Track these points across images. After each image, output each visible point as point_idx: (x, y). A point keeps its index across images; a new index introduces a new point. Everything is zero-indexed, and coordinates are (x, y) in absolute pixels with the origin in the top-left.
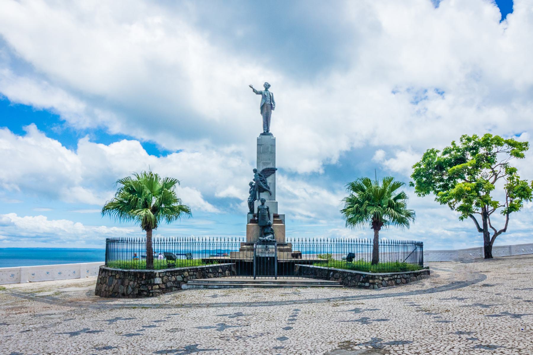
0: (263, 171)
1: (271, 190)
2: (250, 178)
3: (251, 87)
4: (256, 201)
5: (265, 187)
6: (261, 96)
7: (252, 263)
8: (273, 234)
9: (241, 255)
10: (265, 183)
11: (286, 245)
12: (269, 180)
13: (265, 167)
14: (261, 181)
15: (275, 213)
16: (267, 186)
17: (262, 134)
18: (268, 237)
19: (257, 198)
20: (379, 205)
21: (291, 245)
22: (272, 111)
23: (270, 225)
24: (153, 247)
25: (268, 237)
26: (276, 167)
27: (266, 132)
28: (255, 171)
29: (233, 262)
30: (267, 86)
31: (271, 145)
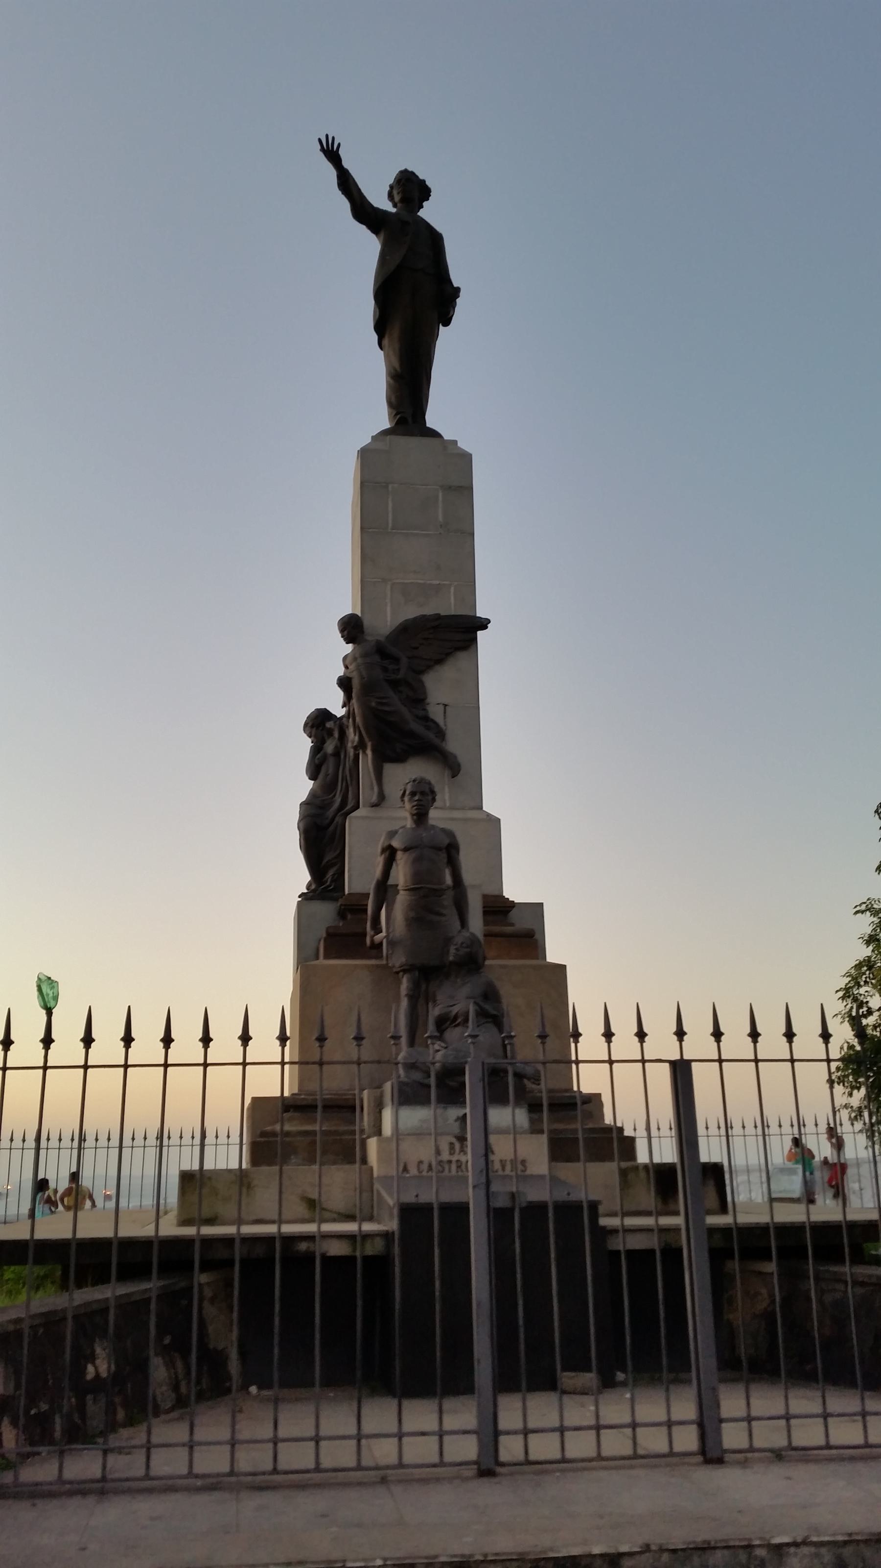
0: (407, 630)
1: (453, 745)
2: (319, 677)
3: (332, 154)
5: (417, 727)
7: (393, 1233)
9: (265, 1198)
10: (418, 700)
12: (438, 686)
13: (411, 612)
14: (394, 684)
15: (490, 890)
16: (426, 720)
17: (385, 433)
18: (470, 1046)
20: (499, 1085)
22: (442, 328)
26: (481, 612)
27: (49, 1012)
28: (351, 628)
29: (128, 1273)
31: (448, 489)
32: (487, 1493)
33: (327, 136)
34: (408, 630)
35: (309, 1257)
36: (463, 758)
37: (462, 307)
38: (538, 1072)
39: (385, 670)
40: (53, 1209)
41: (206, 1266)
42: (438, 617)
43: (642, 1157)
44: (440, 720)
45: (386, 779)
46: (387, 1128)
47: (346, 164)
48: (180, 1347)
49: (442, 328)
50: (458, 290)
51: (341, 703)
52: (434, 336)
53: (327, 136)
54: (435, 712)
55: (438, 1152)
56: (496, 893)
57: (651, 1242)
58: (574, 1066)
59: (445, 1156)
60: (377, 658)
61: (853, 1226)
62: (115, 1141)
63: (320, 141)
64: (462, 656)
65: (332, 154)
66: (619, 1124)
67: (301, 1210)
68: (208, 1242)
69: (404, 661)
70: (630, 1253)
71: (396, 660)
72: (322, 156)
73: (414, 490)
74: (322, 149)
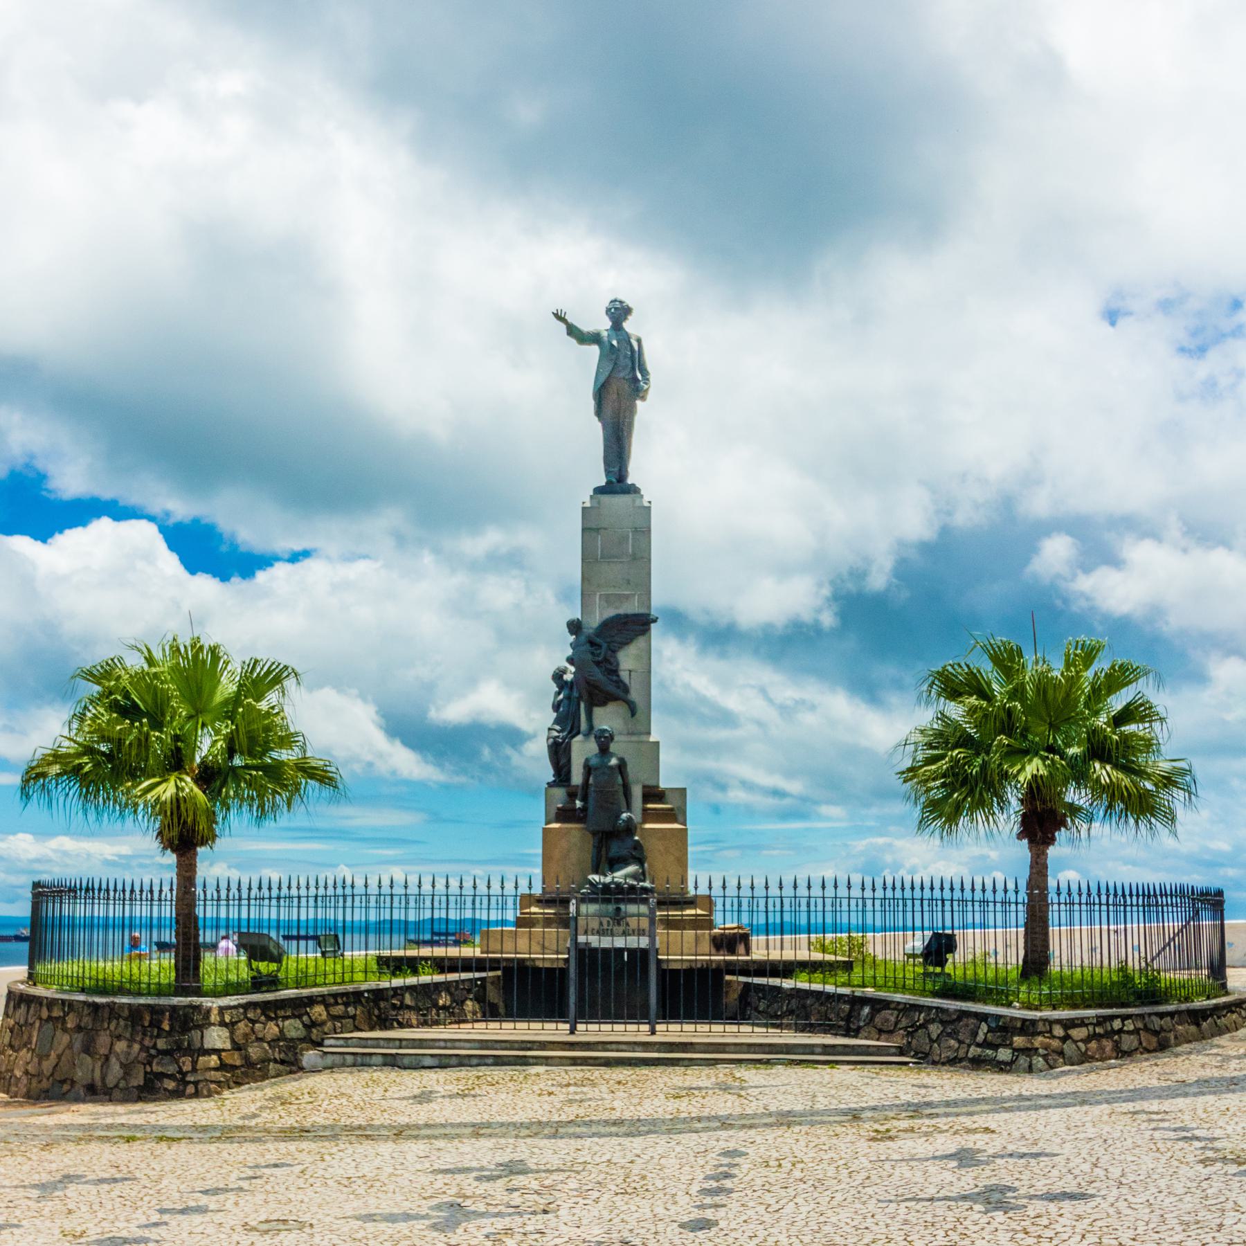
0: (607, 625)
1: (634, 695)
3: (559, 317)
4: (579, 738)
6: (595, 350)
8: (640, 861)
9: (523, 943)
11: (691, 903)
12: (627, 660)
13: (611, 612)
15: (651, 783)
17: (599, 491)
19: (584, 726)
21: (709, 902)
22: (639, 403)
23: (630, 828)
24: (199, 912)
25: (620, 876)
30: (619, 312)
31: (636, 530)
34: (608, 626)
35: (527, 968)
39: (593, 653)
40: (468, 927)
42: (627, 616)
44: (627, 681)
49: (639, 403)
52: (632, 410)
55: (601, 924)
59: (605, 927)
60: (588, 646)
61: (785, 962)
67: (538, 949)
68: (492, 960)
69: (605, 646)
71: (600, 646)
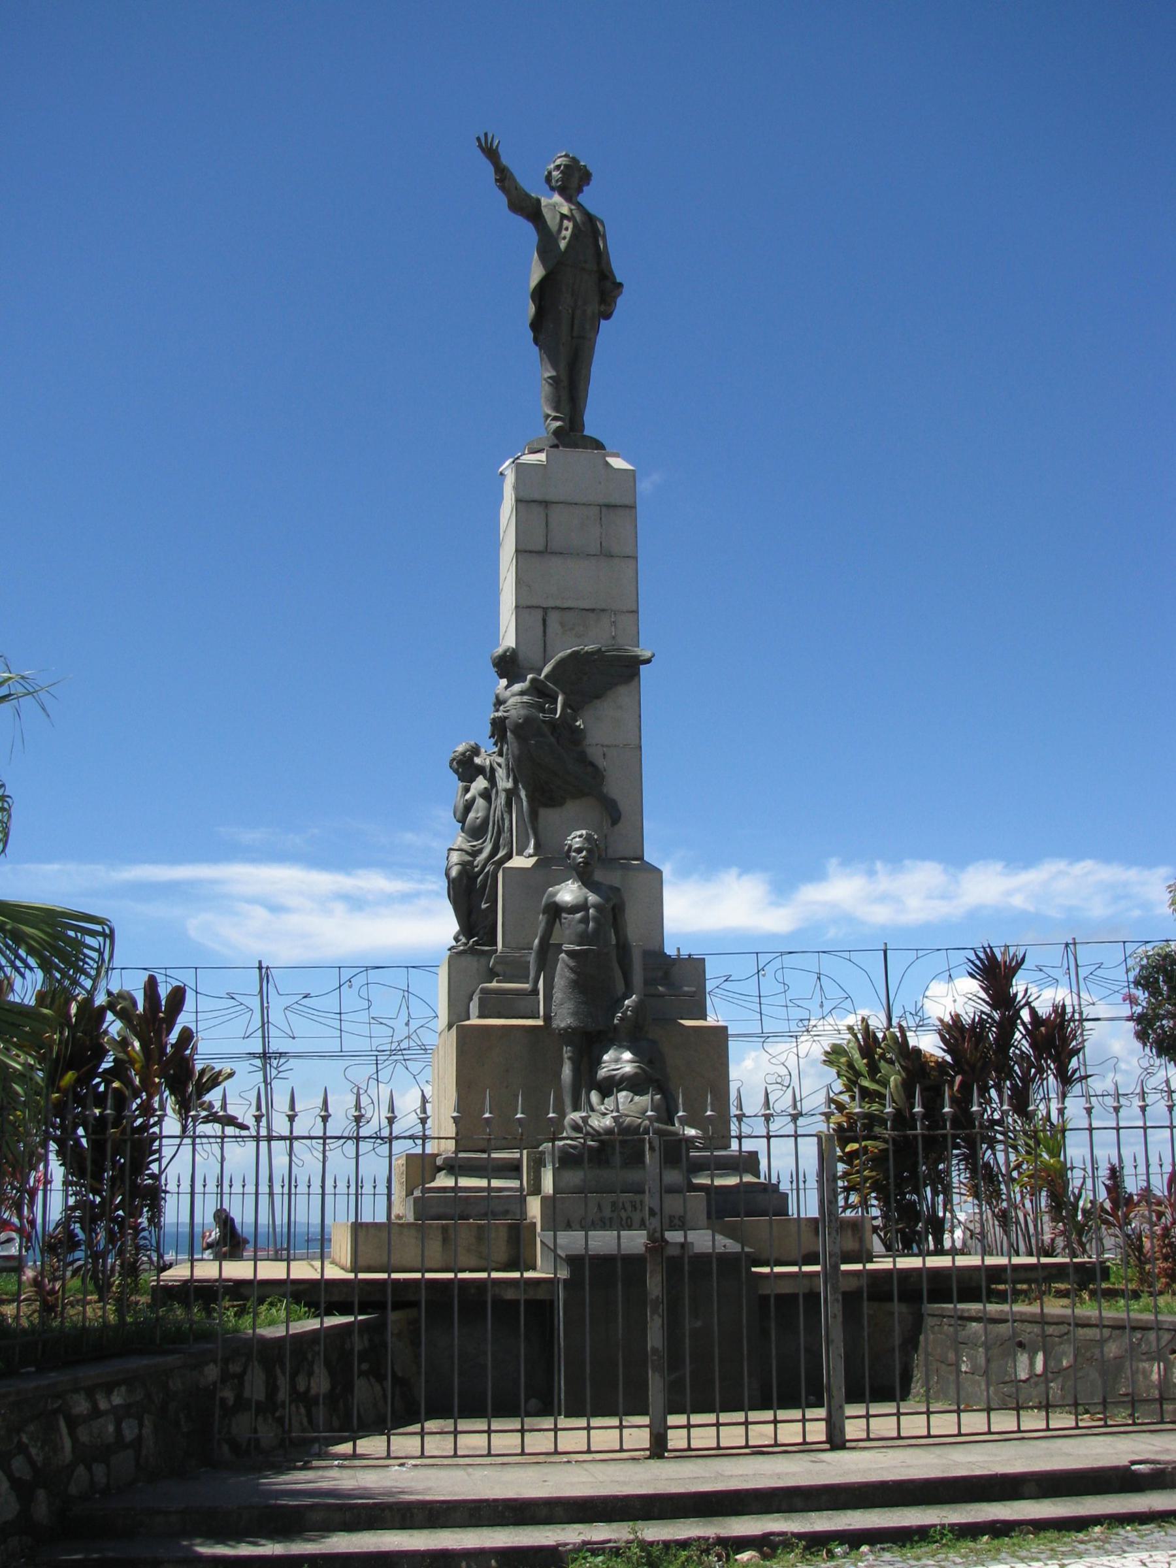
1: (614, 788)
3: (491, 153)
22: (602, 322)
32: (656, 1466)
33: (486, 135)
36: (624, 806)
37: (622, 303)
38: (754, 1155)
41: (397, 1306)
43: (792, 1210)
45: (541, 819)
46: (548, 1186)
47: (505, 160)
48: (377, 1374)
49: (602, 322)
50: (620, 285)
51: (489, 734)
53: (486, 135)
54: (594, 754)
56: (657, 948)
57: (801, 1289)
58: (615, 1421)
62: (316, 1188)
63: (478, 139)
64: (622, 690)
65: (491, 153)
66: (774, 1181)
70: (779, 1297)
72: (479, 151)
73: (578, 531)
74: (480, 146)
